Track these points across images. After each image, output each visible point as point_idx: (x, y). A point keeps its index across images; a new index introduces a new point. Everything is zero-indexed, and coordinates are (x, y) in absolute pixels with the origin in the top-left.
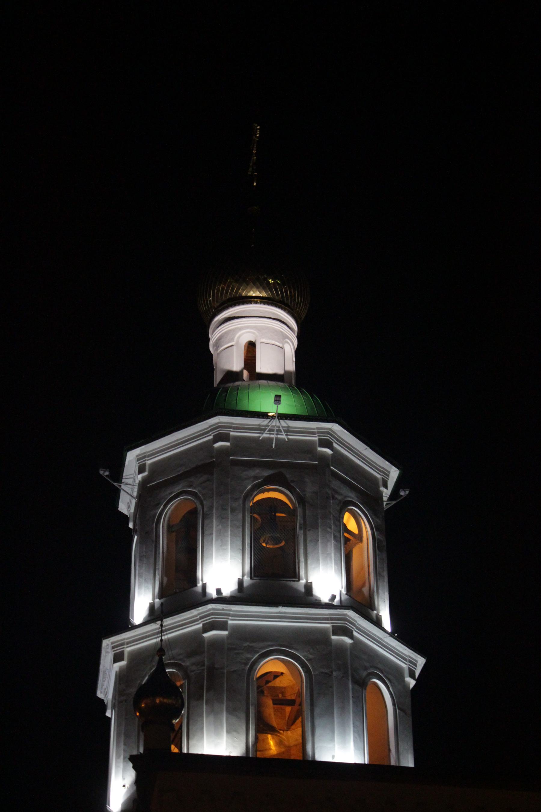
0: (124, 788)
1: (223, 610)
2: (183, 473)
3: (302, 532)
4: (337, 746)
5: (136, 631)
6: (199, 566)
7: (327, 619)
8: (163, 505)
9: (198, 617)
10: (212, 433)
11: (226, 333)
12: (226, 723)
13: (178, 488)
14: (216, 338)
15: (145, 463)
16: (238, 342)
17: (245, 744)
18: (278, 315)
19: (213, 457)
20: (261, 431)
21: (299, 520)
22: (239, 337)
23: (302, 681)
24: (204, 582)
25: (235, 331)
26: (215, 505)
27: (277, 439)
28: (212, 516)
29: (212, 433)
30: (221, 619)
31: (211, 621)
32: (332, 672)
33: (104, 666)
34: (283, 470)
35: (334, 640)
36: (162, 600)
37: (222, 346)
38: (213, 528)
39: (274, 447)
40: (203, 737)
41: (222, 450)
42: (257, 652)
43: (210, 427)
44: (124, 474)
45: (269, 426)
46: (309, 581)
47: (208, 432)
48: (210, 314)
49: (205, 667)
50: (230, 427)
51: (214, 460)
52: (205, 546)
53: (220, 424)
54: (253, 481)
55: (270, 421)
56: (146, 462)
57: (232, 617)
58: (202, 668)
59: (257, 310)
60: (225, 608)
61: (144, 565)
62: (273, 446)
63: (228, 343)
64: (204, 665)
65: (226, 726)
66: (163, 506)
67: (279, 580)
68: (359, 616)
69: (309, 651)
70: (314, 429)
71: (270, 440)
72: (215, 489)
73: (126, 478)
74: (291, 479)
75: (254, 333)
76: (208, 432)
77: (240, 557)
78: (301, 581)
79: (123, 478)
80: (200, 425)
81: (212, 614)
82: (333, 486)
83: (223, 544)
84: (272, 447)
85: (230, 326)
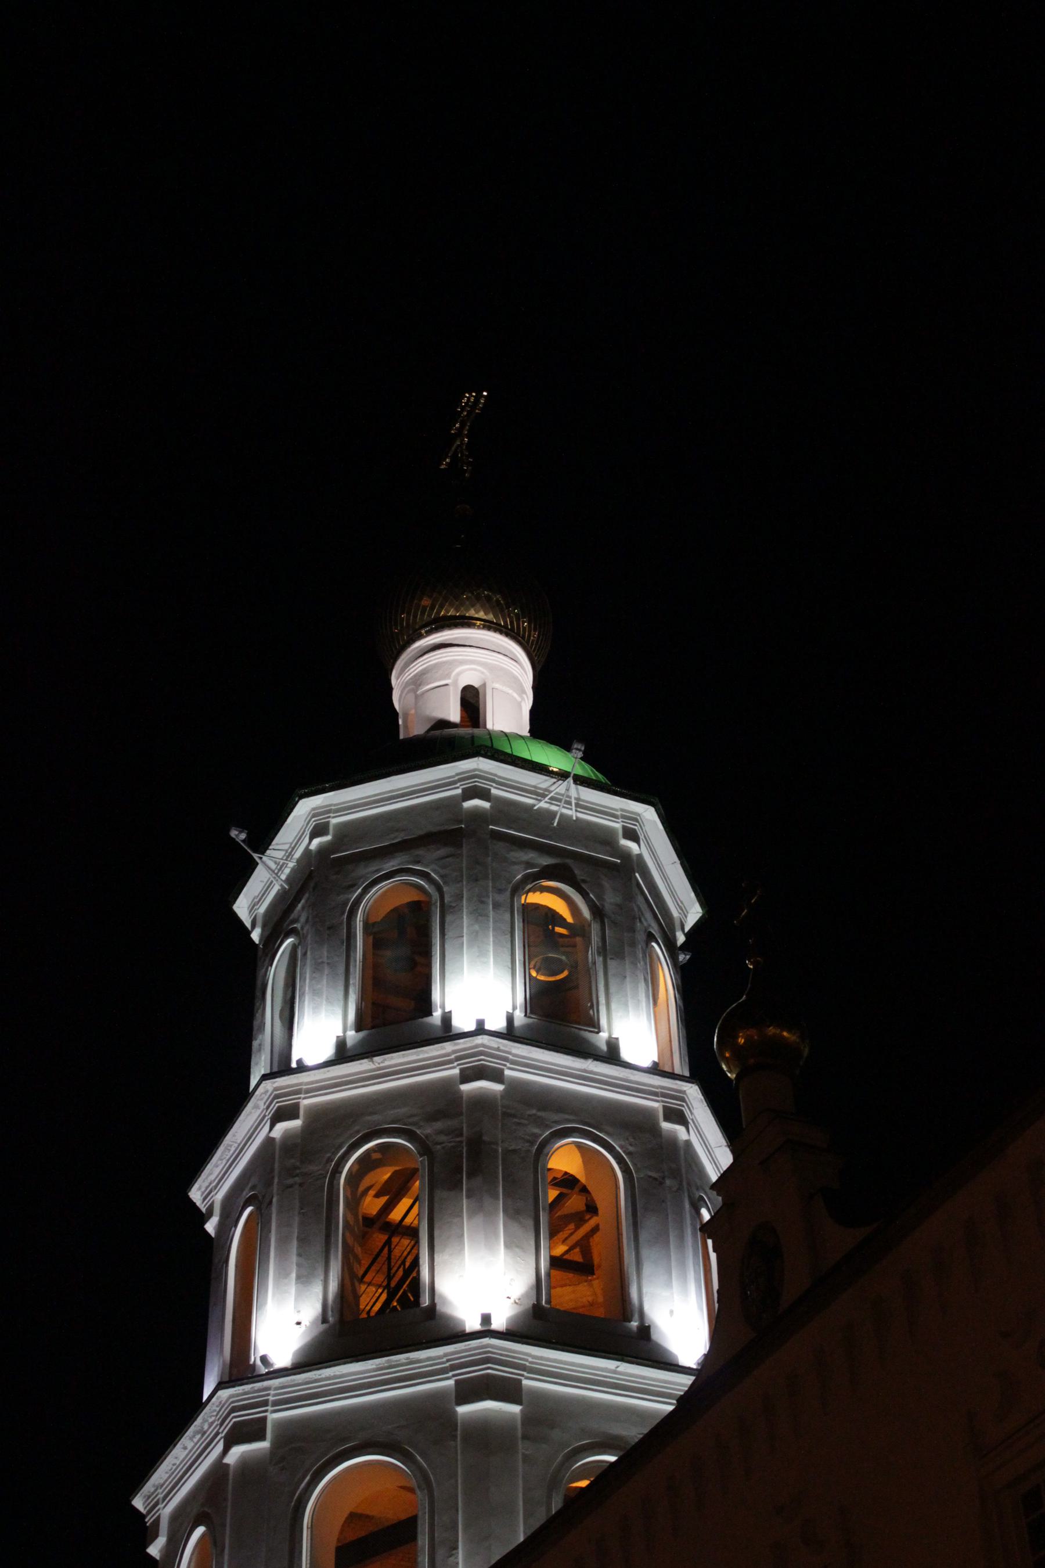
0: (299, 1326)
1: (498, 1049)
2: (399, 843)
3: (601, 959)
4: (675, 1296)
5: (328, 1071)
6: (436, 983)
7: (656, 1094)
8: (361, 888)
9: (453, 1057)
10: (461, 785)
11: (435, 666)
12: (504, 1231)
13: (391, 864)
14: (416, 672)
15: (328, 823)
16: (456, 682)
17: (534, 1270)
18: (517, 657)
19: (461, 822)
20: (537, 795)
21: (595, 939)
22: (458, 674)
23: (617, 1187)
24: (447, 1010)
25: (452, 664)
26: (465, 892)
27: (562, 815)
28: (461, 910)
29: (461, 785)
30: (493, 1063)
31: (478, 1065)
32: (664, 1178)
33: (234, 1136)
34: (568, 861)
35: (664, 1129)
36: (362, 1034)
37: (428, 684)
38: (462, 928)
39: (555, 824)
40: (463, 1249)
41: (477, 814)
42: (548, 1127)
43: (457, 774)
44: (274, 842)
45: (550, 792)
46: (613, 1036)
47: (455, 782)
48: (399, 643)
49: (464, 1139)
50: (493, 781)
51: (463, 826)
52: (447, 953)
53: (477, 772)
54: (527, 869)
55: (554, 783)
56: (330, 819)
57: (511, 1064)
58: (458, 1139)
59: (488, 641)
60: (502, 1048)
61: (325, 977)
62: (554, 823)
63: (440, 680)
64: (461, 1135)
65: (504, 1238)
66: (362, 889)
67: (565, 1025)
68: (702, 1098)
69: (627, 1139)
70: (616, 810)
71: (552, 815)
72: (464, 870)
73: (274, 849)
74: (582, 878)
75: (483, 673)
76: (455, 782)
77: (509, 978)
78: (601, 1034)
79: (271, 847)
80: (442, 769)
81: (481, 1053)
82: (639, 903)
83: (482, 954)
84: (553, 824)
85: (444, 655)
